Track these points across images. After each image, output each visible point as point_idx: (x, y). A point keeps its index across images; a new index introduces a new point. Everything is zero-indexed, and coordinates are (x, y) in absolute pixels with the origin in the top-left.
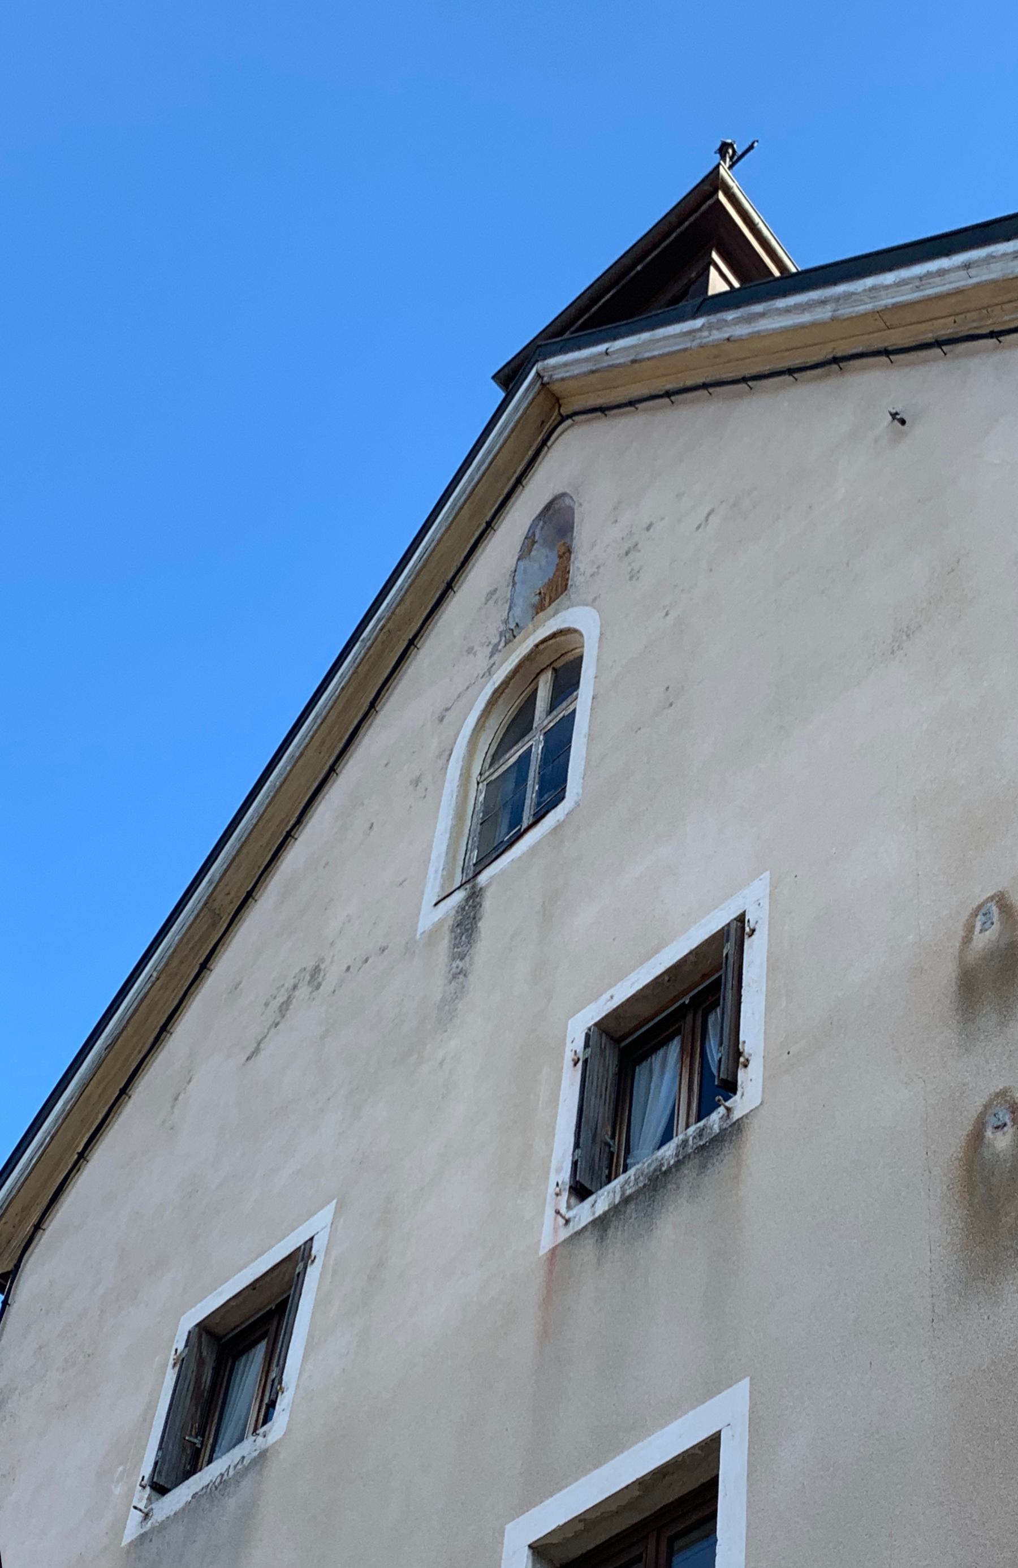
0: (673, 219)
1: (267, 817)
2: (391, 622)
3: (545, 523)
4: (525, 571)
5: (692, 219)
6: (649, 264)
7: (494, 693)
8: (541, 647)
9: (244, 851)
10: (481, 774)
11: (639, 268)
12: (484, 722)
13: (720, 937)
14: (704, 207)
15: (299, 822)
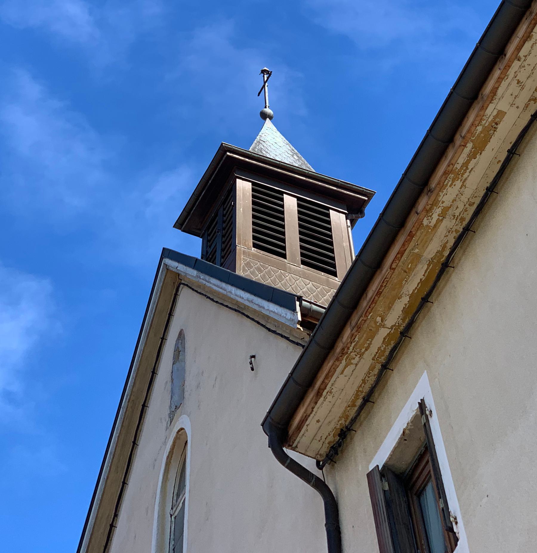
0: (185, 214)
1: (100, 515)
2: (132, 396)
3: (182, 340)
4: (178, 370)
5: (221, 163)
6: (213, 179)
7: (167, 459)
8: (180, 433)
9: (93, 540)
10: (172, 509)
11: (210, 182)
12: (167, 476)
13: (415, 420)
14: (224, 158)
15: (116, 515)
